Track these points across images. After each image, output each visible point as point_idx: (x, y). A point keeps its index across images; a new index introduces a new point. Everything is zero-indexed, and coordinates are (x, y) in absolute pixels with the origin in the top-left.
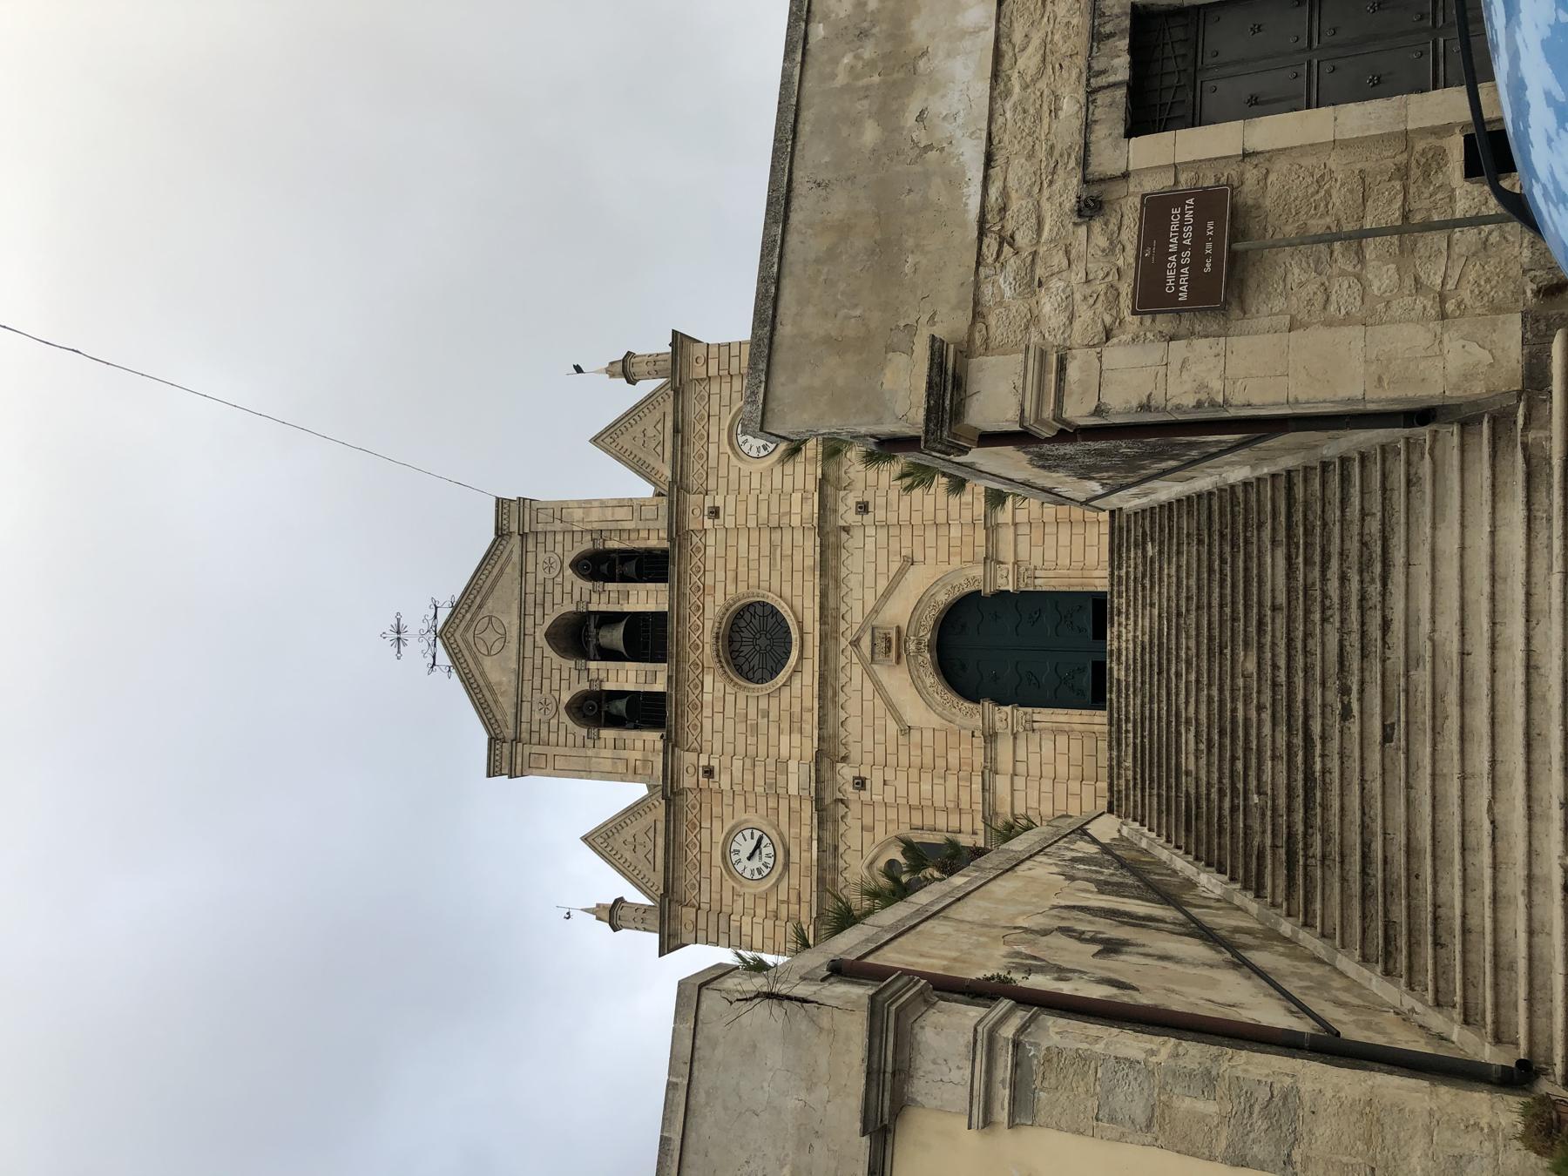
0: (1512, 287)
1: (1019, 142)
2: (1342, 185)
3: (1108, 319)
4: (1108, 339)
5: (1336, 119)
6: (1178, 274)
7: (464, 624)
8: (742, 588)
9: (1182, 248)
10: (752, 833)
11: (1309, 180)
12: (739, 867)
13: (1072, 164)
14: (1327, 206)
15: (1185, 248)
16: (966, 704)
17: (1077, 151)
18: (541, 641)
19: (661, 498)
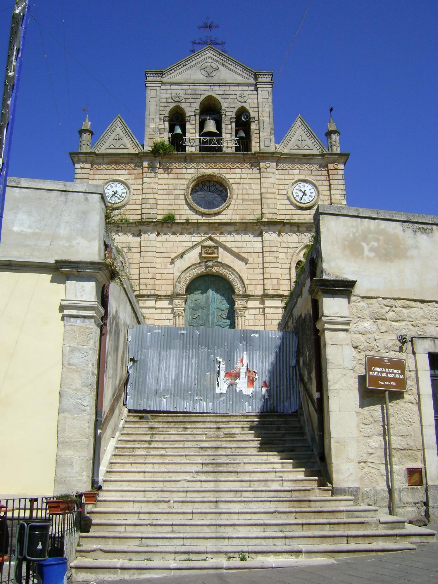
0: (368, 484)
1: (428, 313)
2: (407, 429)
3: (361, 347)
4: (354, 348)
5: (430, 426)
6: (378, 372)
7: (214, 57)
8: (234, 187)
9: (387, 373)
10: (124, 193)
11: (409, 417)
12: (109, 187)
13: (419, 333)
14: (400, 424)
15: (387, 375)
16: (185, 288)
17: (423, 335)
18: (208, 93)
19: (274, 148)
